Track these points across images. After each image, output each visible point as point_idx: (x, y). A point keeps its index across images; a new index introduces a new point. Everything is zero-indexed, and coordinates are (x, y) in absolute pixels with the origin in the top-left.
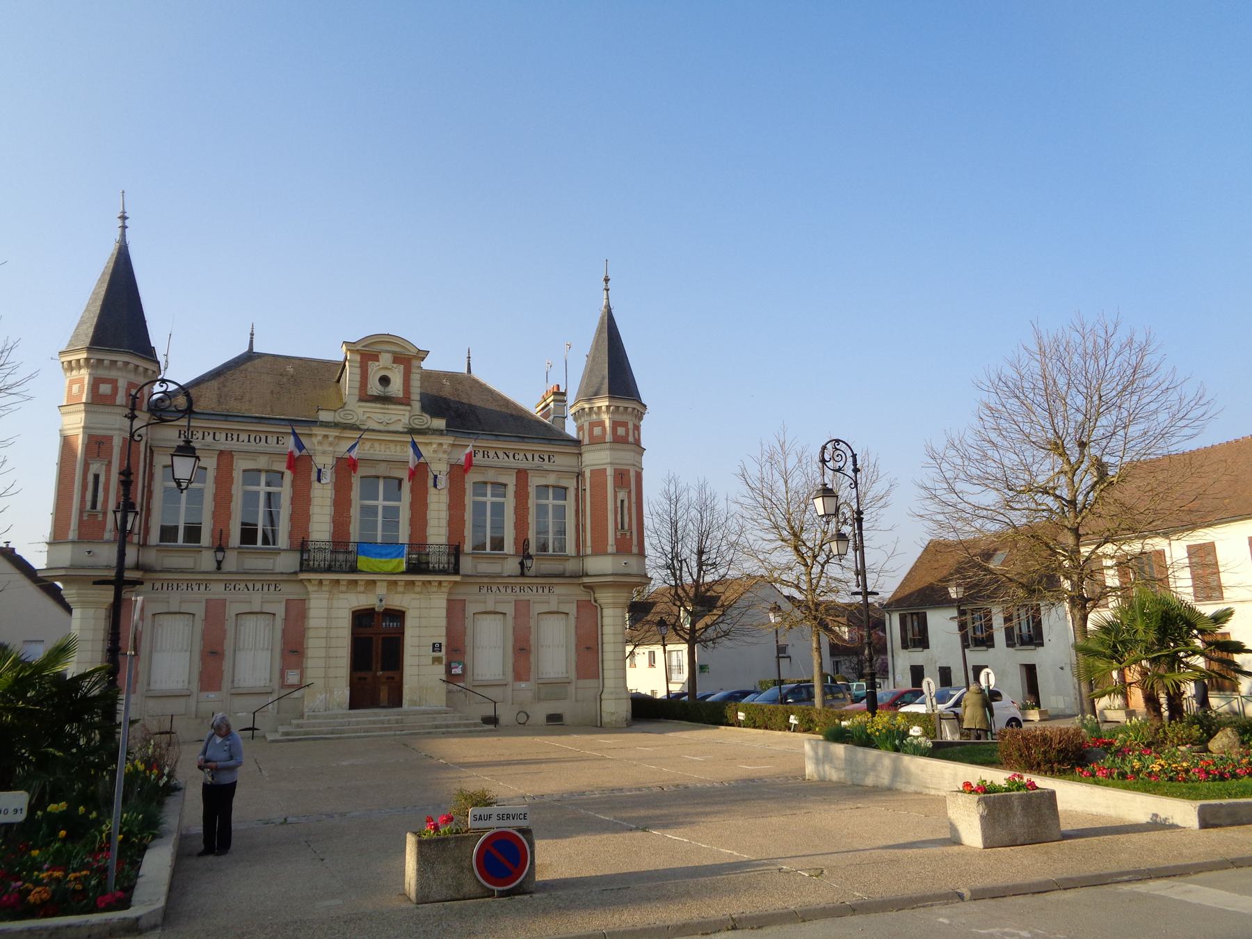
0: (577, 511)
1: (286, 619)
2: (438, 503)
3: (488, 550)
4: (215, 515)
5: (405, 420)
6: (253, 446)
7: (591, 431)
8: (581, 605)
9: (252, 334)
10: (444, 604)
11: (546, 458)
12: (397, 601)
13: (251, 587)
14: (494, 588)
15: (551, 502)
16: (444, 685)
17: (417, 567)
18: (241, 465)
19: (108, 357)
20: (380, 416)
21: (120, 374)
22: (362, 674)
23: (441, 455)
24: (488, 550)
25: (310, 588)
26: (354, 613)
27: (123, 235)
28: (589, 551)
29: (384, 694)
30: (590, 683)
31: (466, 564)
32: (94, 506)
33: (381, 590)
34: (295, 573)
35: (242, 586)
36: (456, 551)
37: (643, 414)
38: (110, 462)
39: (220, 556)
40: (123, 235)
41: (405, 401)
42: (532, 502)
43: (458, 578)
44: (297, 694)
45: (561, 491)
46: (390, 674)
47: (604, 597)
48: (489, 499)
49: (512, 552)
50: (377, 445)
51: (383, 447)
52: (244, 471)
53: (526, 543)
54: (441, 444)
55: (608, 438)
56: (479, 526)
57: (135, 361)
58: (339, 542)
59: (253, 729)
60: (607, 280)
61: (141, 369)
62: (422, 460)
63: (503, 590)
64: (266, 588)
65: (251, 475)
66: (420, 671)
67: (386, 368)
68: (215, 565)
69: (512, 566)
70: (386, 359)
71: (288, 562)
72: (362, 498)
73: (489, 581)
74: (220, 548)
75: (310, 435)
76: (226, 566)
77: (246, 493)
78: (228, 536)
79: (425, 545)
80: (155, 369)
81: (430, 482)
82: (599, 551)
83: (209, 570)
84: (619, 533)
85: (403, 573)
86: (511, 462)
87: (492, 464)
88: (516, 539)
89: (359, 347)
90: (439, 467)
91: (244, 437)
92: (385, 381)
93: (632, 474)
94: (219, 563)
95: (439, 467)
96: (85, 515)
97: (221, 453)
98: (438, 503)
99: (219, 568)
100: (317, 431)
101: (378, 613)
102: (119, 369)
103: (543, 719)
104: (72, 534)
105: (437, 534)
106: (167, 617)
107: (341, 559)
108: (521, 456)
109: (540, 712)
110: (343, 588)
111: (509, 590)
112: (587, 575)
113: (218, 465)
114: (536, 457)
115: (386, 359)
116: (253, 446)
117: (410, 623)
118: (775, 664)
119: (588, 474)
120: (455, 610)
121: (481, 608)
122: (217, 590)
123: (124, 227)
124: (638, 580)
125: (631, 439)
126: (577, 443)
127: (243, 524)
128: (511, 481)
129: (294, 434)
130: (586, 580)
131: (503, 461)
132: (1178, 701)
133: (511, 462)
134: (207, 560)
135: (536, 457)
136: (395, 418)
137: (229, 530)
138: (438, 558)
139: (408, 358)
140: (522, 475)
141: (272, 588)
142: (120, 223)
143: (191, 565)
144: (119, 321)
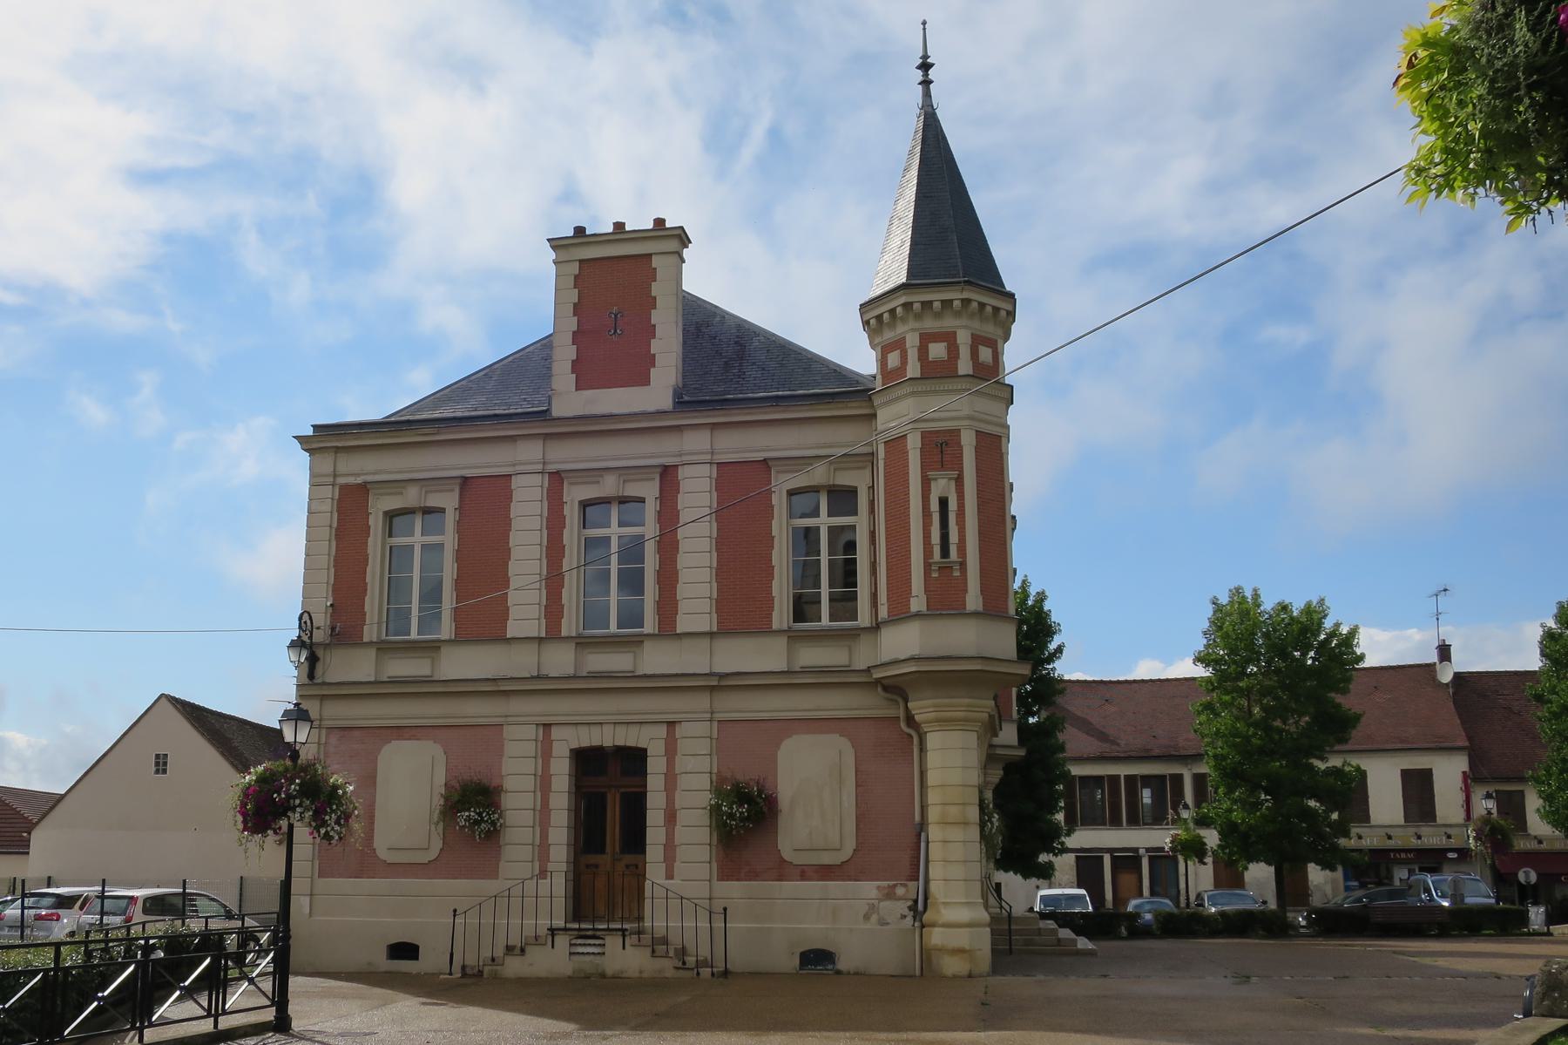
3: (825, 620)
19: (936, 296)
21: (958, 322)
22: (593, 859)
24: (825, 620)
27: (927, 95)
32: (945, 552)
37: (1011, 315)
40: (927, 95)
42: (571, 536)
46: (629, 858)
55: (913, 369)
57: (977, 296)
61: (989, 309)
80: (1010, 308)
93: (968, 441)
102: (958, 314)
118: (1461, 797)
123: (926, 83)
128: (649, 490)
130: (877, 675)
132: (2, 948)
143: (630, 668)
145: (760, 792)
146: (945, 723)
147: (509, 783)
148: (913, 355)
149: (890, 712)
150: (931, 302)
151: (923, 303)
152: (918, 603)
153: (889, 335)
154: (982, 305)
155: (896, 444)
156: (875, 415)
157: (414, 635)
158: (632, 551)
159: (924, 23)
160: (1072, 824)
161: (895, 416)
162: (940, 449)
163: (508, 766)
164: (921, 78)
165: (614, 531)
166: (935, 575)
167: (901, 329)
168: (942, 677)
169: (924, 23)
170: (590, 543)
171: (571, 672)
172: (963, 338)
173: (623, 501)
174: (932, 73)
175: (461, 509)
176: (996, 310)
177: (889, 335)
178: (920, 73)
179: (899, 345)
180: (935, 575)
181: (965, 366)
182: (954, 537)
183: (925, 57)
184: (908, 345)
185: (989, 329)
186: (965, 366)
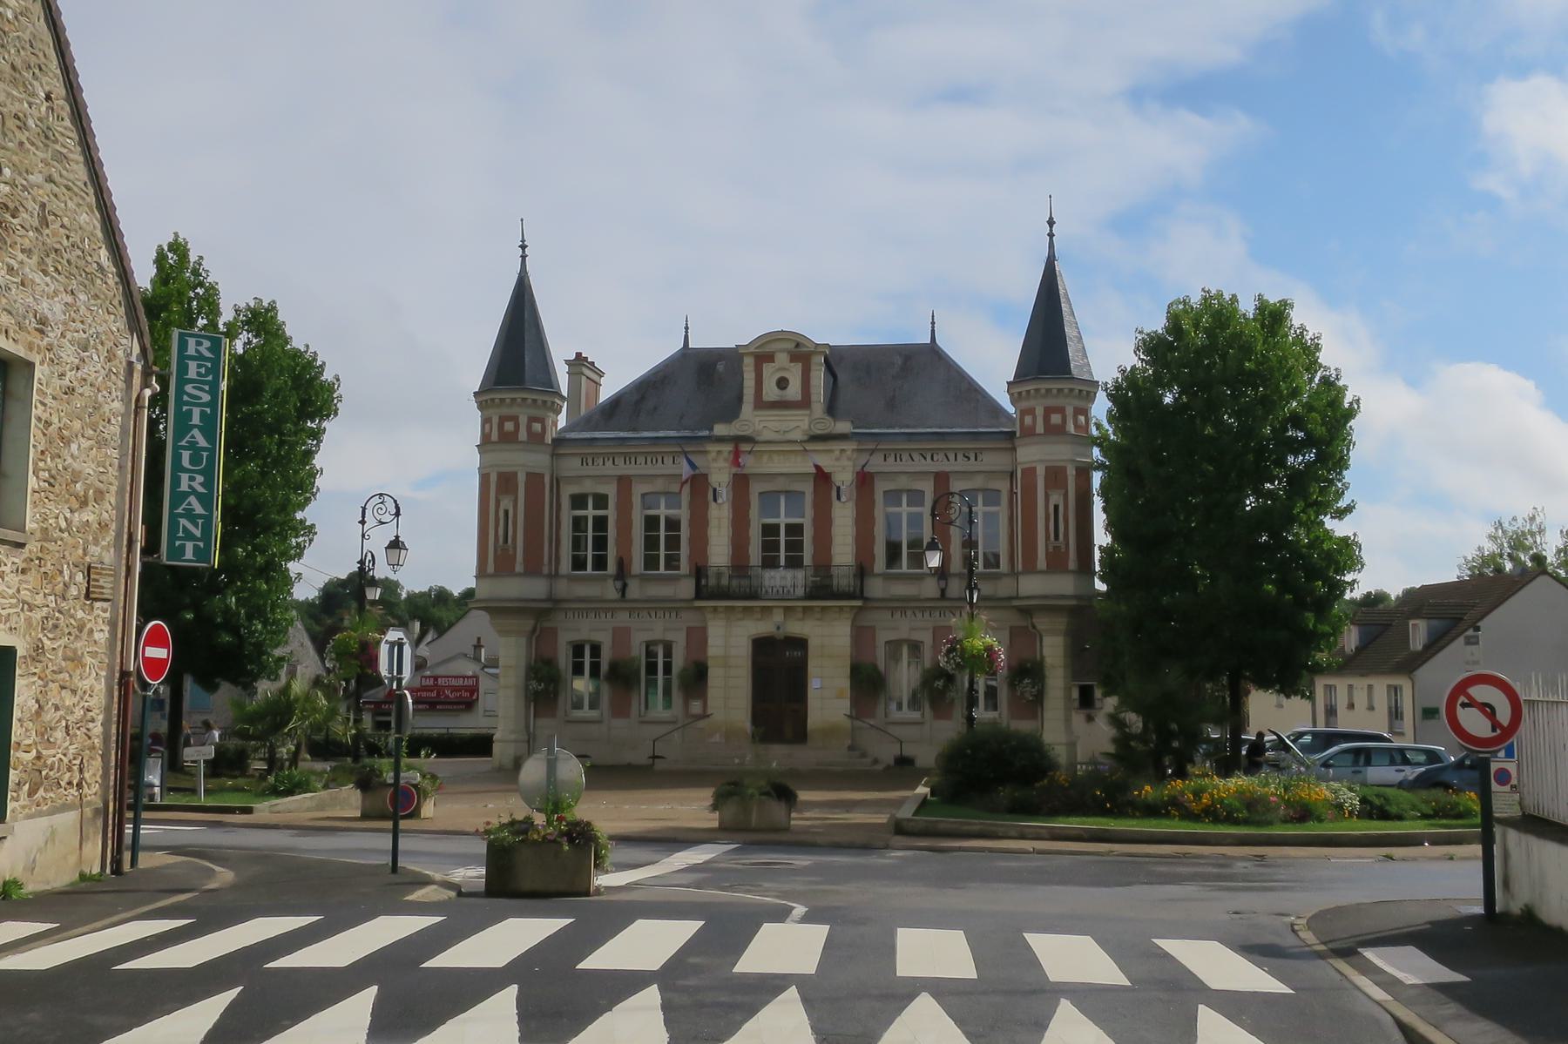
5: (805, 425)
7: (501, 426)
8: (1015, 633)
10: (848, 630)
12: (796, 628)
15: (905, 509)
17: (822, 590)
23: (845, 463)
24: (905, 569)
25: (709, 616)
31: (875, 588)
32: (506, 541)
33: (778, 617)
36: (862, 571)
39: (942, 584)
41: (805, 403)
43: (858, 603)
44: (702, 724)
45: (601, 501)
47: (1042, 622)
48: (590, 512)
50: (775, 458)
54: (842, 451)
55: (1040, 429)
57: (1055, 386)
58: (739, 565)
63: (919, 615)
67: (784, 369)
70: (782, 359)
71: (686, 588)
72: (921, 514)
73: (902, 606)
77: (887, 516)
79: (828, 567)
81: (834, 494)
82: (1030, 568)
85: (799, 599)
89: (752, 349)
90: (844, 477)
91: (641, 459)
92: (782, 383)
93: (1071, 472)
94: (943, 591)
95: (844, 477)
100: (713, 448)
104: (490, 569)
105: (843, 552)
111: (927, 614)
112: (1017, 598)
114: (960, 456)
115: (782, 359)
116: (972, 465)
120: (861, 636)
122: (622, 619)
123: (524, 257)
125: (1071, 428)
128: (928, 487)
129: (685, 453)
130: (1016, 603)
134: (610, 591)
135: (960, 456)
136: (793, 425)
138: (842, 577)
147: (1048, 661)
148: (1040, 421)
149: (1023, 624)
152: (1042, 563)
153: (1025, 404)
155: (1030, 473)
156: (1014, 449)
157: (905, 569)
160: (378, 681)
162: (1055, 476)
163: (1046, 652)
165: (663, 512)
168: (1049, 607)
172: (523, 420)
177: (1025, 404)
179: (1031, 411)
181: (523, 435)
185: (1080, 404)
186: (523, 435)
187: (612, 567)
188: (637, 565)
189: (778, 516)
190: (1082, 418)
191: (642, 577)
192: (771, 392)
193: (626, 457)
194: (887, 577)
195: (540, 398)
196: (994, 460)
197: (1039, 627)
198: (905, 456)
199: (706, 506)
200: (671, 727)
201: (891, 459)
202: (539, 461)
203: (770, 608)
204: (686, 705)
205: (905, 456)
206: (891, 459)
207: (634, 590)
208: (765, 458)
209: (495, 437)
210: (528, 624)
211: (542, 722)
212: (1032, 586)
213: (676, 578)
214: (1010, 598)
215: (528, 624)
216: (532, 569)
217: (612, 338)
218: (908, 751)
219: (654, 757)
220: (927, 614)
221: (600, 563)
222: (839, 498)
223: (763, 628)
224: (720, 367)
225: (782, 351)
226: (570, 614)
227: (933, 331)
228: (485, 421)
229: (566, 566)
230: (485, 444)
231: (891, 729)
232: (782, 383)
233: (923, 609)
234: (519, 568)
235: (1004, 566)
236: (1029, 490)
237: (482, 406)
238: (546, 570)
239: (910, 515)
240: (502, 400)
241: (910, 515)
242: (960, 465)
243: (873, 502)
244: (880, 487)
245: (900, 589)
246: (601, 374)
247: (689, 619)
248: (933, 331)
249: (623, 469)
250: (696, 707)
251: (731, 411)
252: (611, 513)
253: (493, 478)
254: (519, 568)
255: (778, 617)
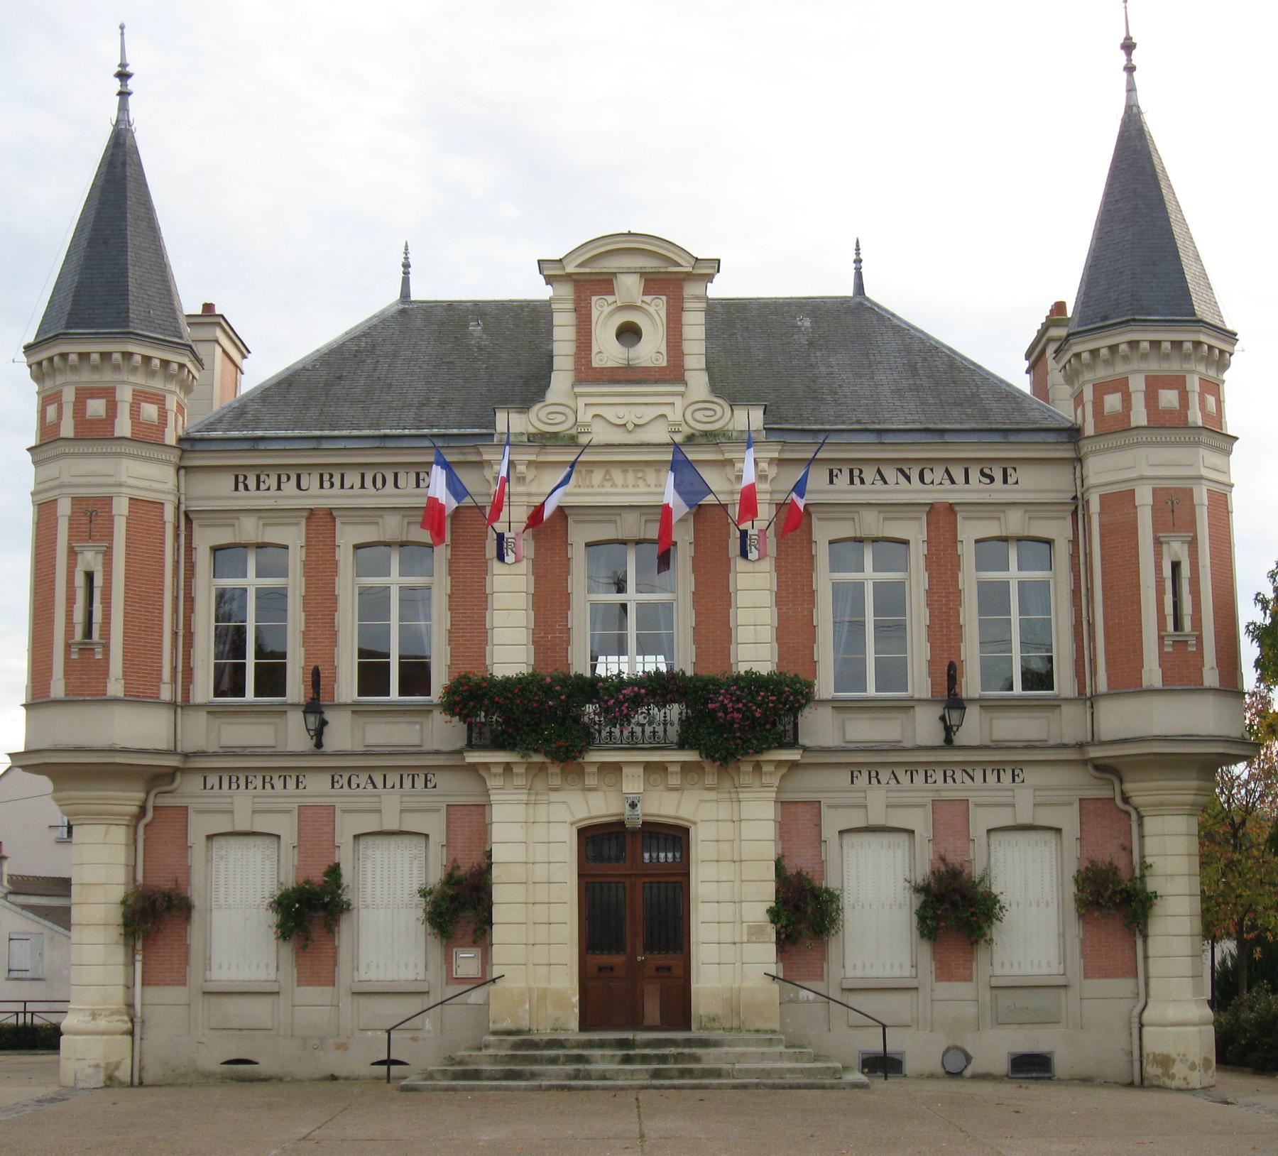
0: (1076, 592)
1: (448, 845)
2: (754, 589)
4: (454, 635)
6: (370, 498)
9: (406, 266)
11: (998, 476)
12: (663, 805)
13: (379, 780)
14: (885, 775)
16: (775, 987)
18: (969, 531)
20: (622, 411)
25: (492, 783)
26: (581, 832)
27: (123, 108)
28: (1102, 686)
29: (652, 1009)
30: (1122, 986)
32: (88, 633)
33: (633, 783)
34: (460, 752)
35: (363, 779)
38: (110, 548)
39: (954, 716)
40: (123, 108)
41: (673, 373)
42: (969, 578)
43: (794, 755)
44: (476, 997)
46: (659, 959)
47: (1141, 790)
49: (926, 693)
50: (617, 475)
51: (631, 477)
52: (357, 547)
53: (953, 674)
55: (1139, 416)
56: (995, 640)
57: (1166, 336)
59: (389, 1062)
60: (1128, 46)
62: (467, 501)
63: (904, 778)
64: (407, 782)
65: (994, 548)
66: (729, 949)
68: (943, 735)
69: (926, 726)
70: (630, 286)
73: (868, 762)
74: (314, 706)
75: (480, 464)
76: (959, 739)
77: (983, 586)
78: (334, 679)
82: (1127, 682)
83: (936, 744)
84: (1168, 642)
86: (913, 491)
87: (873, 498)
88: (931, 663)
89: (570, 269)
91: (353, 478)
92: (629, 333)
94: (949, 731)
96: (1168, 642)
97: (312, 513)
98: (754, 589)
99: (948, 741)
101: (634, 832)
103: (1003, 1066)
104: (58, 688)
106: (378, 840)
107: (540, 720)
108: (939, 474)
109: (994, 1048)
110: (674, 781)
111: (919, 778)
113: (308, 538)
114: (974, 475)
115: (630, 286)
116: (997, 492)
117: (700, 849)
119: (1095, 507)
120: (798, 819)
121: (221, 824)
122: (317, 786)
123: (1130, 69)
124: (173, 762)
125: (1195, 417)
126: (1073, 433)
127: (362, 653)
128: (915, 531)
129: (446, 466)
130: (1094, 753)
131: (900, 490)
133: (913, 491)
134: (295, 732)
135: (974, 475)
137: (334, 668)
139: (672, 275)
140: (942, 518)
141: (420, 782)
142: (1122, 58)
144: (112, 270)
145: (982, 879)
146: (1161, 808)
148: (1138, 402)
149: (1105, 793)
150: (88, 354)
151: (102, 354)
152: (1152, 673)
154: (1211, 348)
155: (1119, 502)
156: (1080, 460)
157: (871, 691)
158: (891, 599)
159: (122, 27)
161: (1104, 469)
164: (118, 88)
165: (251, 582)
166: (75, 656)
167: (60, 380)
169: (122, 27)
170: (983, 586)
171: (163, 746)
173: (261, 546)
174: (131, 83)
175: (308, 545)
176: (1222, 352)
178: (117, 82)
180: (75, 656)
181: (124, 426)
182: (1187, 607)
183: (1128, 38)
184: (64, 399)
187: (296, 688)
188: (347, 686)
189: (877, 586)
190: (1211, 400)
191: (357, 710)
192: (607, 351)
193: (325, 473)
194: (840, 706)
195: (158, 354)
196: (1038, 483)
197: (1137, 800)
198: (870, 474)
199: (483, 570)
200: (415, 1005)
201: (842, 480)
202: (150, 477)
203: (617, 767)
204: (448, 960)
205: (870, 474)
206: (842, 480)
207: (342, 733)
208: (598, 476)
209: (67, 430)
210: (128, 798)
211: (155, 993)
212: (1121, 719)
213: (281, 711)
214: (1080, 746)
215: (128, 798)
216: (140, 694)
217: (276, 286)
218: (896, 1044)
219: (389, 1062)
220: (919, 778)
221: (272, 680)
222: (744, 554)
223: (600, 805)
224: (475, 328)
225: (630, 272)
226: (213, 780)
227: (858, 261)
228: (47, 399)
229: (203, 688)
230: (47, 444)
231: (855, 1000)
232: (629, 333)
233: (912, 768)
234: (115, 687)
235: (1064, 681)
236: (1120, 534)
237: (40, 372)
238: (166, 694)
239: (262, 594)
240: (84, 356)
241: (262, 594)
242: (976, 490)
243: (811, 558)
244: (823, 532)
245: (864, 730)
246: (244, 351)
247: (453, 788)
248: (858, 261)
249: (316, 496)
250: (467, 961)
251: (532, 387)
252: (295, 584)
253: (64, 508)
254: (115, 687)
255: (633, 783)
